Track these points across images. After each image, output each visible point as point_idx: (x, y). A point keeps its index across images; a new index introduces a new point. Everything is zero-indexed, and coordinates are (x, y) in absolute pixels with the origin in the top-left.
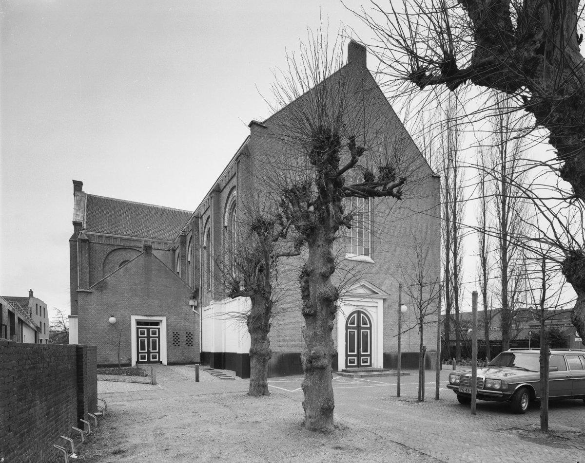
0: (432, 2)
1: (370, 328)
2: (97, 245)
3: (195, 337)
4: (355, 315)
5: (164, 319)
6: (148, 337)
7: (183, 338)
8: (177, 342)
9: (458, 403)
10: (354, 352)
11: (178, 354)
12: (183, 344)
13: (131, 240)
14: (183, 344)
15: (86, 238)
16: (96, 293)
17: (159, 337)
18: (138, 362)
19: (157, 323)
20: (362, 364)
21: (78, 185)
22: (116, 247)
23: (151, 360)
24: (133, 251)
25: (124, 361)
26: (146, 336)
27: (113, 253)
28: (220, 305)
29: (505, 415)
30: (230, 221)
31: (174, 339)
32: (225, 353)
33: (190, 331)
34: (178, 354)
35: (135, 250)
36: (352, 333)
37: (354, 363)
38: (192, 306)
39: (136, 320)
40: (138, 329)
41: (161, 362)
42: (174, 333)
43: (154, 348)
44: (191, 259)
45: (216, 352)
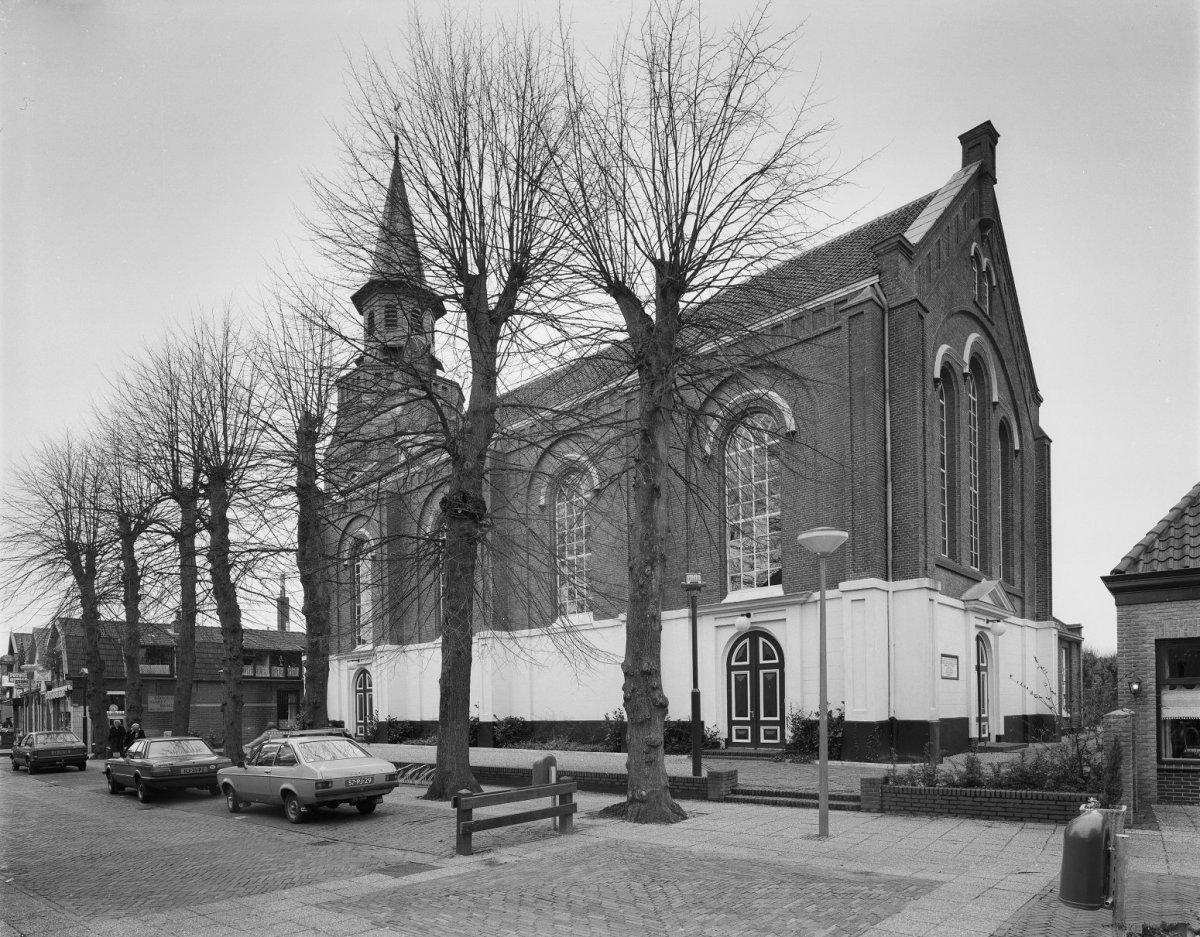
1: (781, 665)
4: (747, 641)
6: (755, 667)
26: (747, 663)
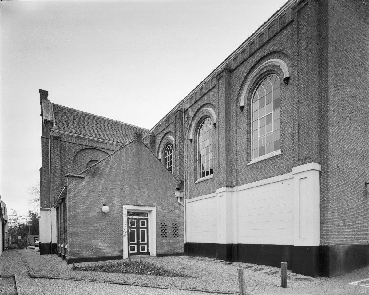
2: (67, 144)
3: (180, 228)
5: (154, 210)
6: (138, 228)
7: (170, 229)
8: (165, 232)
9: (40, 250)
11: (165, 245)
12: (170, 234)
13: (98, 142)
14: (170, 234)
15: (58, 135)
16: (88, 178)
17: (147, 228)
18: (129, 254)
19: (145, 214)
21: (44, 94)
22: (84, 147)
23: (141, 251)
24: (99, 151)
25: (116, 254)
27: (82, 152)
28: (230, 193)
30: (248, 100)
31: (162, 230)
32: (238, 245)
33: (176, 223)
34: (165, 245)
35: (102, 151)
38: (177, 198)
39: (128, 209)
40: (128, 219)
41: (149, 254)
42: (162, 224)
43: (143, 240)
44: (162, 156)
45: (228, 243)
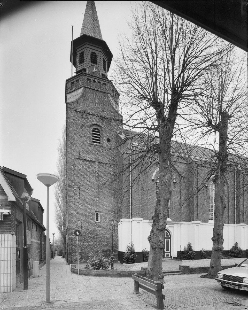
0: (247, 267)
1: (170, 238)
10: (169, 250)
20: (166, 257)
29: (227, 293)
36: (167, 241)
37: (168, 256)
43: (167, 250)
